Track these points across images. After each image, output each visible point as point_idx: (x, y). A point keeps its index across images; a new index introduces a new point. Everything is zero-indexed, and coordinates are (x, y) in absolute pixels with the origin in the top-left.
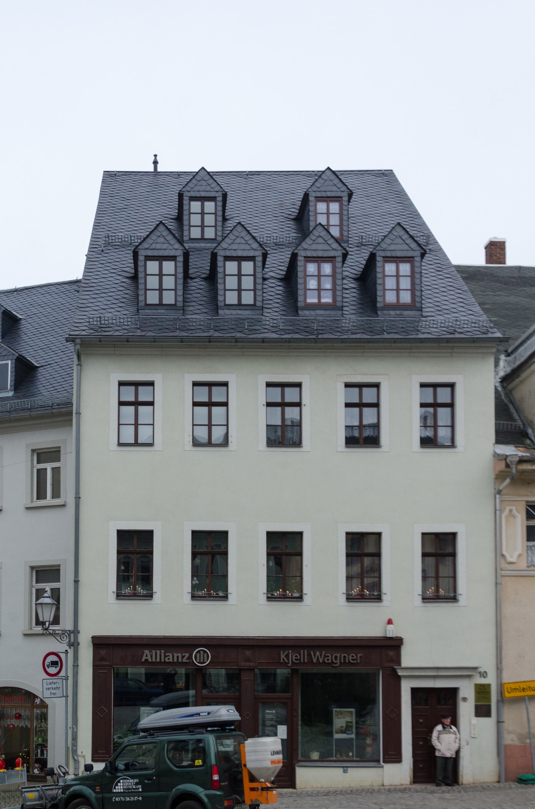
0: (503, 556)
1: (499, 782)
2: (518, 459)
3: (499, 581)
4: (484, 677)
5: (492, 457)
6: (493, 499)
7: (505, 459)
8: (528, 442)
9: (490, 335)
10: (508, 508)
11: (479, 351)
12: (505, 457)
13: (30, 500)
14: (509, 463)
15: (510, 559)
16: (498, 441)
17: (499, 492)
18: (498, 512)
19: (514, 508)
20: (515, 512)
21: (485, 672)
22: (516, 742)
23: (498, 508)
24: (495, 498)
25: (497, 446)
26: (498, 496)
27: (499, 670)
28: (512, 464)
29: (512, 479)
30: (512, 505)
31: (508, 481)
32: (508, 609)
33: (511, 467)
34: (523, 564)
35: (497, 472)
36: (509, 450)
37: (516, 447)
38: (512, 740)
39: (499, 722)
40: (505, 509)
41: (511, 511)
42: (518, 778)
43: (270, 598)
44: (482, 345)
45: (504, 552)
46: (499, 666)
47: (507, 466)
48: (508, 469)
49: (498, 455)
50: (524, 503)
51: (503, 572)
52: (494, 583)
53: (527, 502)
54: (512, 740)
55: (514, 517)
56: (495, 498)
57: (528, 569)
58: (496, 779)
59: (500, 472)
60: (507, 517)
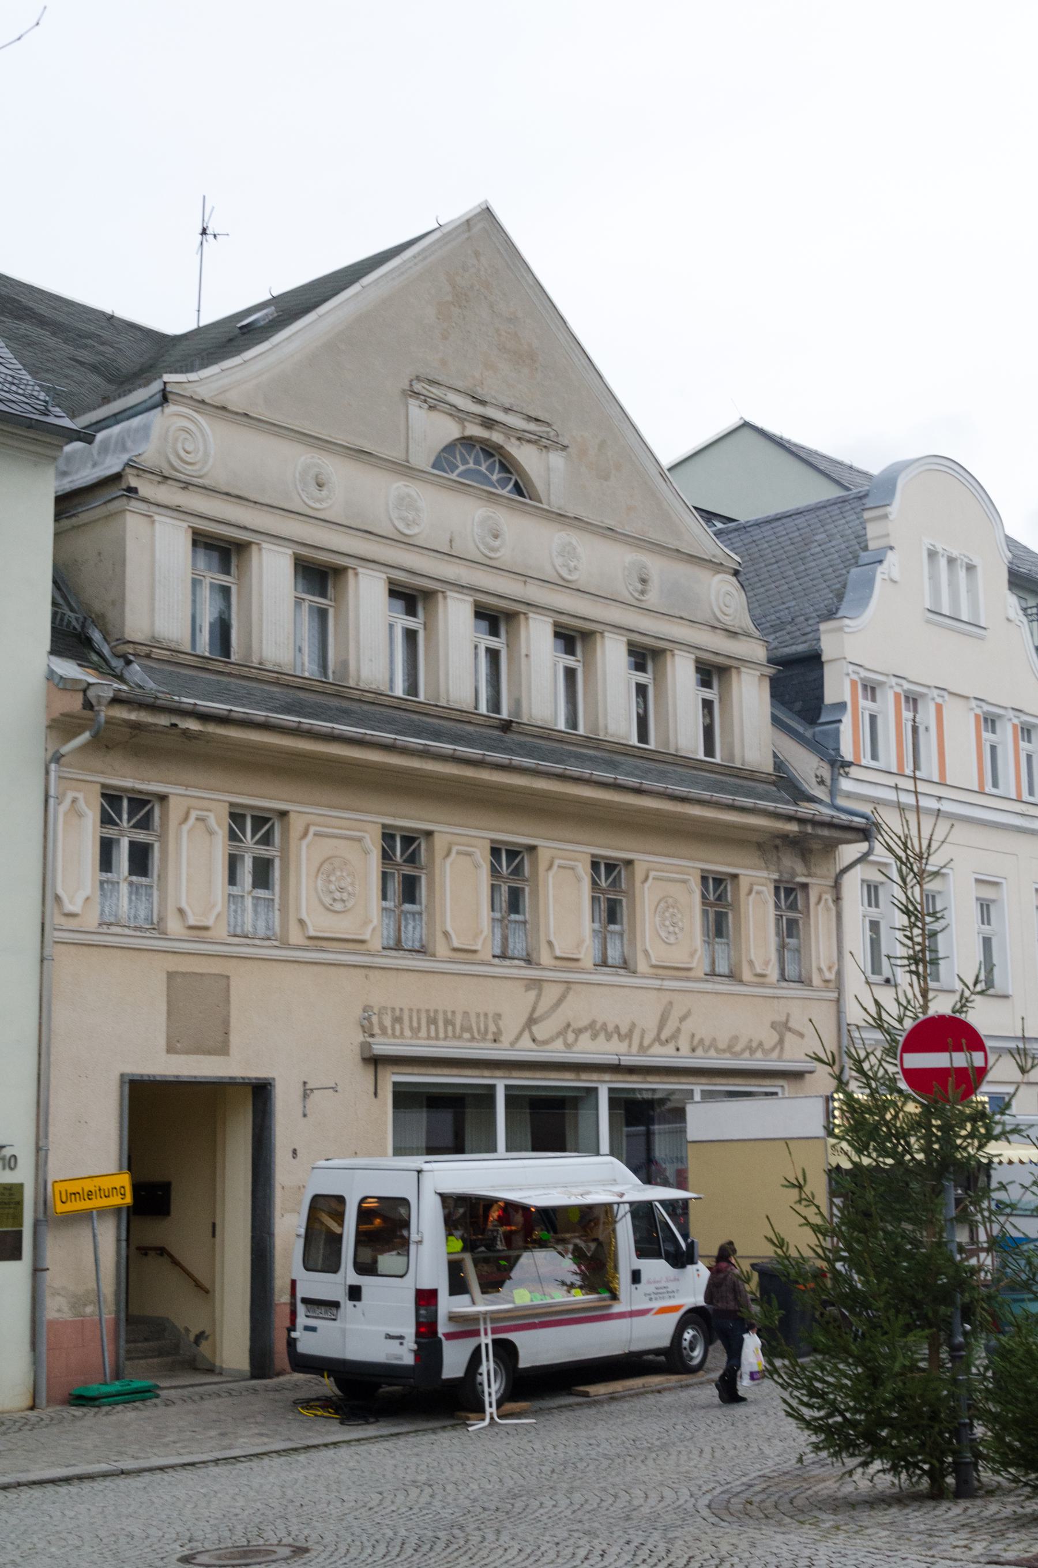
0: (58, 898)
1: (32, 1408)
2: (111, 695)
3: (47, 953)
4: (11, 1169)
5: (43, 680)
6: (43, 771)
7: (85, 691)
8: (95, 658)
9: (51, 420)
10: (70, 795)
11: (32, 448)
12: (84, 686)
13: (669, 466)
14: (94, 701)
15: (69, 907)
16: (56, 650)
17: (57, 758)
18: (52, 801)
19: (80, 796)
20: (82, 804)
21: (15, 1156)
22: (67, 1315)
23: (52, 792)
24: (47, 772)
25: (53, 658)
26: (53, 766)
27: (40, 1151)
28: (99, 703)
29: (95, 736)
30: (79, 791)
31: (86, 736)
32: (61, 1016)
33: (96, 708)
34: (91, 921)
35: (56, 715)
36: (68, 668)
37: (80, 665)
38: (59, 1311)
39: (37, 1270)
40: (64, 795)
41: (74, 801)
42: (70, 1395)
43: (122, 1075)
44: (39, 438)
45: (60, 892)
46: (41, 1144)
47: (88, 705)
48: (88, 713)
49: (61, 677)
50: (98, 787)
51: (57, 934)
52: (39, 959)
53: (104, 786)
54: (59, 1311)
55: (80, 815)
56: (47, 772)
57: (101, 930)
58: (27, 1402)
59: (62, 714)
60: (66, 814)
